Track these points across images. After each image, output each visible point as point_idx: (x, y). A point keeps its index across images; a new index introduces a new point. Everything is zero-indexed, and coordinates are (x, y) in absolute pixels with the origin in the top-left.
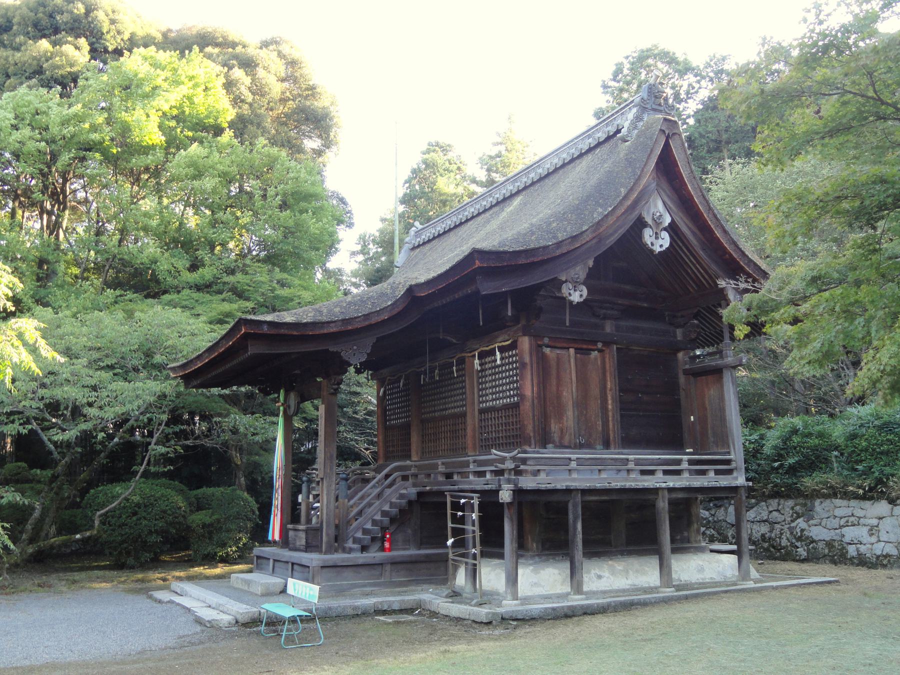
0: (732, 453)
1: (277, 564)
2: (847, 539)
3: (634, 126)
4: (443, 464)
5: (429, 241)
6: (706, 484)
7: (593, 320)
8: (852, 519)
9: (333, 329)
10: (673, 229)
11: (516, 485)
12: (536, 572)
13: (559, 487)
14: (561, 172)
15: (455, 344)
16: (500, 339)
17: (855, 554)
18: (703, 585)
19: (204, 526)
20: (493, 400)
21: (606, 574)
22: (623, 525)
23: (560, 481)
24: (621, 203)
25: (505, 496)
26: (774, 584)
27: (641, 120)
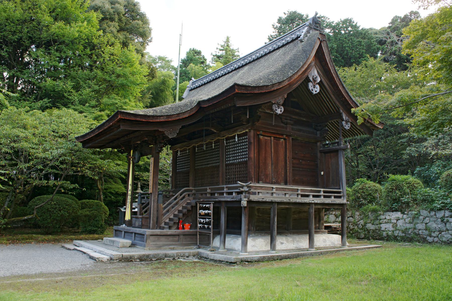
0: (341, 188)
1: (126, 234)
2: (383, 229)
3: (306, 35)
4: (209, 188)
5: (200, 86)
6: (330, 202)
7: (282, 125)
8: (386, 220)
9: (162, 120)
10: (320, 84)
11: (248, 199)
12: (254, 240)
13: (267, 201)
14: (269, 55)
15: (216, 133)
16: (239, 131)
17: (385, 235)
18: (325, 248)
19: (86, 216)
20: (233, 160)
21: (285, 242)
22: (296, 220)
23: (268, 198)
24: (300, 69)
25: (244, 203)
26: (357, 247)
27: (309, 33)
